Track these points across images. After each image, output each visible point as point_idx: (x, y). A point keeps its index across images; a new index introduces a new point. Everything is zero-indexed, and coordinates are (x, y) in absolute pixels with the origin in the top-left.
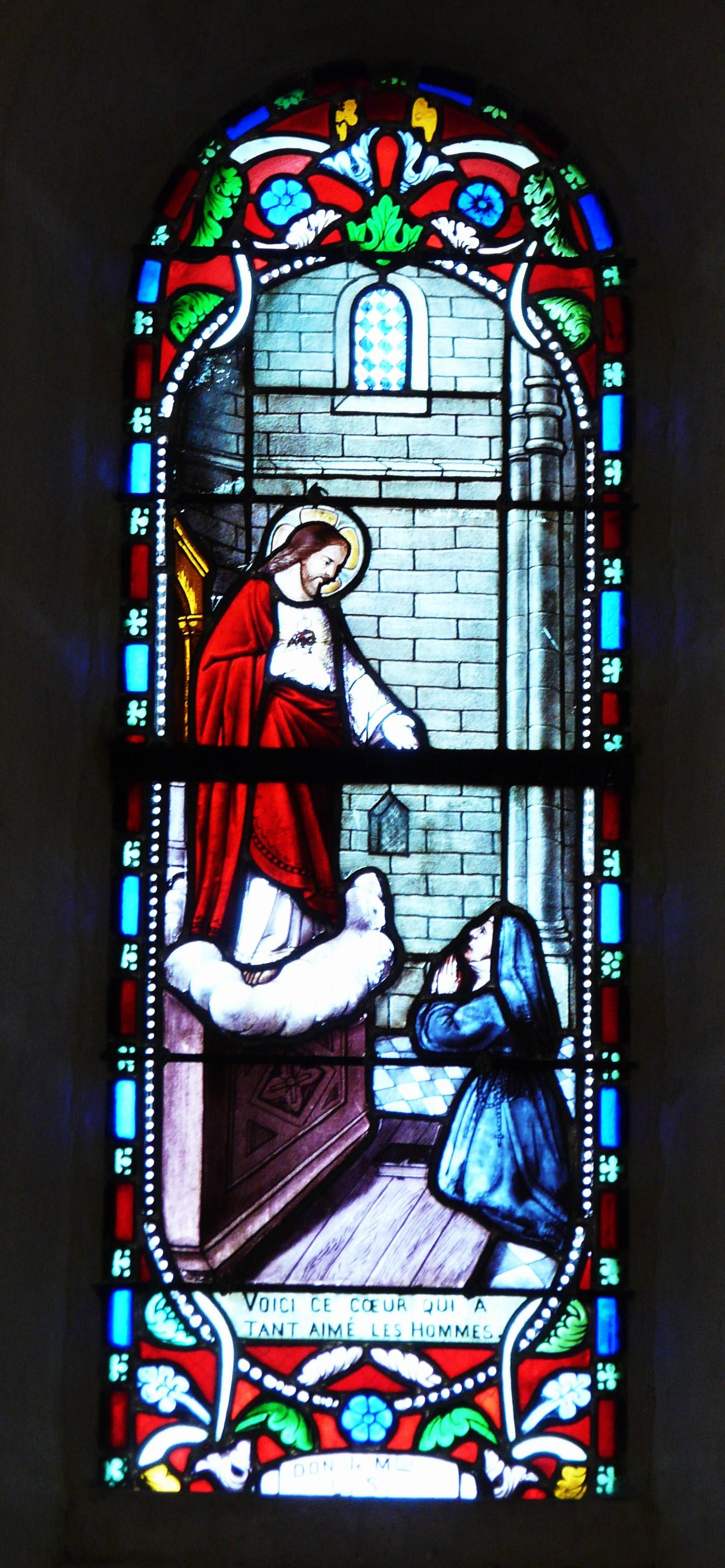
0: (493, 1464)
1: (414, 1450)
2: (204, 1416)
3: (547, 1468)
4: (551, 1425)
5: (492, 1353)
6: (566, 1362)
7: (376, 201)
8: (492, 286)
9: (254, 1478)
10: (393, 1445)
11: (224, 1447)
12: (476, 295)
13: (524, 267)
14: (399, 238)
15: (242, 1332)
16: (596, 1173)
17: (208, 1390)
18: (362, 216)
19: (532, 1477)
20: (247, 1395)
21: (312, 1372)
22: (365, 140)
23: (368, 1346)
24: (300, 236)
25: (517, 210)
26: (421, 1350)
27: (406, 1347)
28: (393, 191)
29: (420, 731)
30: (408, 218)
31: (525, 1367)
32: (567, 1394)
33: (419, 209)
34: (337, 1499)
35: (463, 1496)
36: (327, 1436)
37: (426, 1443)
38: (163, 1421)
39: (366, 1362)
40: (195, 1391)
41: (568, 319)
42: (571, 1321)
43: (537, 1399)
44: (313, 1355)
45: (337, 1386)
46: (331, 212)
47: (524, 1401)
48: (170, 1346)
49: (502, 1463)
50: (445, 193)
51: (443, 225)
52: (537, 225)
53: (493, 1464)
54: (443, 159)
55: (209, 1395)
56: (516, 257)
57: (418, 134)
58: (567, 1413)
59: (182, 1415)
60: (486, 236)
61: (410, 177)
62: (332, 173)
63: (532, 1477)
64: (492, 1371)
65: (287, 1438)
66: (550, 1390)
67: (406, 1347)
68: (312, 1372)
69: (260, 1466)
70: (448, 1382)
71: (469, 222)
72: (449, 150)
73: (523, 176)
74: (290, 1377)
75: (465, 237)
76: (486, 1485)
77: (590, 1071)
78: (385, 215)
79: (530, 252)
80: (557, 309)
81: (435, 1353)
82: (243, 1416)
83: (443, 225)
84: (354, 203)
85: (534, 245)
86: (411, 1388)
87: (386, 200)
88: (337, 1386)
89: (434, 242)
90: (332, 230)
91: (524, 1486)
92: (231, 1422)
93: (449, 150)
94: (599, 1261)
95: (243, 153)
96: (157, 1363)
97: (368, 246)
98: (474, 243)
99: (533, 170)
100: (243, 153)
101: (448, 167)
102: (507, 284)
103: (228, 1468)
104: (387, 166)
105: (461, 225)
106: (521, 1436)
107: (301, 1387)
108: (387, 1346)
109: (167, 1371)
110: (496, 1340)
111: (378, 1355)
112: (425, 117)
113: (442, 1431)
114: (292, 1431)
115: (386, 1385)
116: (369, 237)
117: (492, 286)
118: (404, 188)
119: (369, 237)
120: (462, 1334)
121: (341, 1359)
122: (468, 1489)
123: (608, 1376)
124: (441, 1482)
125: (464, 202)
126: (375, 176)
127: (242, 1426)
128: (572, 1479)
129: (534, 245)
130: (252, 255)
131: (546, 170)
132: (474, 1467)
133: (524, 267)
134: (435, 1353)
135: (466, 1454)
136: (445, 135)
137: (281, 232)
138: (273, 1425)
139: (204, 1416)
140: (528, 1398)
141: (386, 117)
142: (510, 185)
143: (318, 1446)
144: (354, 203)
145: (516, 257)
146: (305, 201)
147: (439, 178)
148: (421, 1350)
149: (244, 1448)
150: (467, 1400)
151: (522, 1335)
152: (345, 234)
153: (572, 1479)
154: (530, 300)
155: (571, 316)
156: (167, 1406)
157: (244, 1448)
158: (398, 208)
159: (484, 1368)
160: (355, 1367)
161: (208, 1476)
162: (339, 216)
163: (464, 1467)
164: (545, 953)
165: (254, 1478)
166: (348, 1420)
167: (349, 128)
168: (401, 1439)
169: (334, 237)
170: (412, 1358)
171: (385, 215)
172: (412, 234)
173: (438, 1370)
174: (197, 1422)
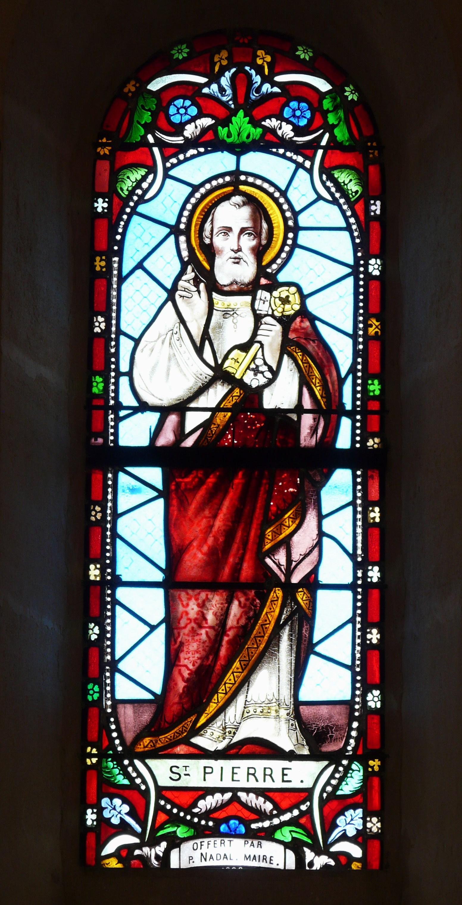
0: (309, 855)
2: (138, 829)
4: (344, 837)
5: (308, 793)
7: (235, 113)
12: (246, 687)
13: (320, 152)
15: (161, 783)
16: (366, 269)
18: (226, 122)
20: (162, 817)
21: (205, 804)
22: (228, 74)
23: (234, 791)
24: (190, 131)
31: (326, 809)
34: (230, 759)
38: (114, 831)
39: (235, 799)
41: (349, 182)
42: (355, 774)
44: (203, 797)
45: (216, 815)
50: (274, 105)
51: (272, 123)
52: (331, 123)
53: (309, 855)
54: (274, 84)
55: (142, 817)
56: (314, 145)
57: (259, 70)
58: (351, 833)
60: (298, 131)
64: (303, 808)
66: (340, 821)
68: (205, 804)
70: (282, 812)
71: (288, 122)
72: (279, 79)
73: (322, 96)
74: (188, 811)
78: (240, 120)
79: (324, 143)
80: (343, 177)
82: (162, 827)
85: (327, 136)
86: (261, 815)
88: (216, 815)
89: (269, 137)
90: (209, 130)
92: (154, 830)
93: (279, 79)
95: (155, 85)
97: (229, 140)
98: (292, 134)
100: (155, 85)
101: (276, 90)
102: (312, 159)
104: (241, 93)
105: (284, 124)
107: (194, 815)
108: (248, 791)
111: (242, 795)
115: (246, 814)
116: (229, 135)
119: (229, 135)
124: (276, 856)
126: (235, 98)
127: (161, 833)
129: (327, 136)
130: (159, 143)
133: (320, 152)
136: (275, 70)
137: (178, 130)
139: (138, 829)
140: (329, 826)
142: (314, 99)
144: (221, 112)
145: (314, 145)
146: (193, 111)
151: (323, 790)
152: (216, 133)
155: (351, 180)
156: (115, 821)
158: (247, 119)
159: (303, 802)
160: (224, 806)
162: (214, 121)
167: (221, 66)
169: (209, 137)
170: (261, 799)
171: (240, 120)
174: (133, 833)
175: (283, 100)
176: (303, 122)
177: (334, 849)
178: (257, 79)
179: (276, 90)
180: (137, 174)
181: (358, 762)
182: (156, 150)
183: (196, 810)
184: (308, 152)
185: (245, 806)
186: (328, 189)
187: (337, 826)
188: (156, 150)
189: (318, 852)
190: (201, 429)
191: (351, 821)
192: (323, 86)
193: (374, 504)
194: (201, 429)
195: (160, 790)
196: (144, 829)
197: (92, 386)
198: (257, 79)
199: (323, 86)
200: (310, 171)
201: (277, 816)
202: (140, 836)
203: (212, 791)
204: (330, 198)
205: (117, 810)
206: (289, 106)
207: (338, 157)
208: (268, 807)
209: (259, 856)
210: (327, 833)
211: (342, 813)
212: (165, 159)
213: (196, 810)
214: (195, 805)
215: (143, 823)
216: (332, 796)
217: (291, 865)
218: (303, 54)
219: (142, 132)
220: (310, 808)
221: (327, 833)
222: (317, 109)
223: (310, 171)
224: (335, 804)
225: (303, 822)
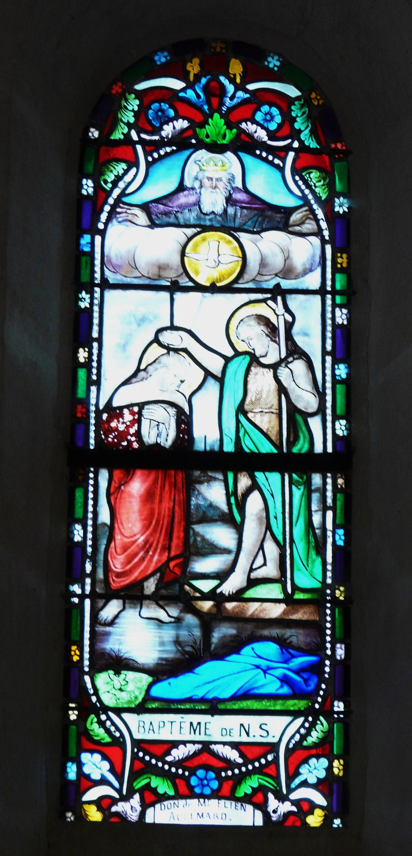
0: (273, 803)
1: (232, 797)
3: (305, 807)
4: (305, 784)
5: (273, 747)
6: (314, 752)
8: (277, 161)
9: (142, 814)
10: (220, 794)
11: (125, 798)
13: (291, 155)
14: (224, 137)
17: (118, 769)
18: (203, 124)
19: (294, 809)
24: (168, 130)
25: (288, 120)
26: (235, 745)
27: (224, 744)
28: (219, 111)
29: (199, 801)
30: (229, 125)
31: (292, 759)
32: (315, 769)
33: (234, 117)
35: (256, 824)
36: (185, 792)
37: (240, 793)
40: (112, 770)
43: (297, 774)
46: (186, 122)
47: (291, 772)
48: (98, 743)
49: (277, 801)
51: (250, 127)
53: (273, 803)
54: (246, 91)
57: (232, 81)
58: (312, 780)
59: (103, 781)
60: (272, 135)
61: (228, 102)
62: (187, 101)
63: (294, 809)
65: (161, 791)
66: (304, 769)
67: (224, 744)
68: (178, 753)
69: (145, 805)
72: (251, 87)
74: (165, 762)
75: (262, 135)
76: (266, 816)
77: (328, 598)
81: (243, 748)
83: (250, 127)
84: (199, 118)
86: (229, 764)
87: (216, 116)
91: (289, 814)
94: (341, 759)
96: (92, 752)
98: (265, 139)
99: (298, 98)
102: (284, 160)
103: (130, 809)
106: (290, 790)
109: (97, 757)
110: (275, 740)
112: (236, 68)
113: (245, 789)
114: (163, 786)
117: (277, 161)
118: (224, 109)
120: (199, 723)
121: (192, 748)
122: (259, 821)
123: (337, 766)
124: (247, 817)
125: (259, 116)
128: (315, 820)
131: (305, 100)
132: (262, 806)
133: (291, 155)
134: (243, 748)
135: (257, 799)
136: (248, 78)
137: (157, 131)
138: (153, 785)
139: (116, 784)
140: (292, 775)
141: (215, 66)
143: (178, 796)
145: (289, 148)
147: (244, 102)
148: (235, 745)
149: (137, 797)
150: (260, 771)
153: (315, 820)
154: (295, 171)
156: (96, 776)
157: (137, 797)
161: (117, 814)
163: (257, 806)
164: (230, 72)
165: (142, 814)
166: (194, 781)
168: (226, 792)
170: (228, 748)
171: (217, 121)
172: (230, 135)
173: (241, 755)
175: (253, 106)
176: (273, 126)
177: (294, 796)
178: (231, 89)
179: (248, 96)
180: (121, 168)
181: (325, 719)
182: (139, 148)
183: (169, 759)
184: (282, 154)
185: (215, 755)
186: (299, 187)
187: (299, 774)
188: (139, 148)
189: (281, 798)
190: (188, 413)
191: (315, 769)
192: (292, 91)
193: (82, 365)
194: (188, 413)
195: (136, 743)
196: (121, 785)
197: (345, 535)
198: (231, 89)
199: (292, 91)
200: (281, 170)
201: (245, 764)
202: (119, 791)
203: (185, 743)
204: (300, 195)
205: (94, 765)
206: (260, 111)
207: (306, 158)
208: (233, 755)
209: (200, 734)
210: (290, 778)
211: (305, 761)
212: (147, 153)
213: (169, 759)
214: (169, 754)
215: (120, 778)
216: (298, 744)
217: (259, 821)
218: (273, 63)
219: (126, 130)
220: (276, 759)
221: (290, 778)
222: (286, 114)
223: (281, 170)
224: (299, 754)
225: (269, 770)
